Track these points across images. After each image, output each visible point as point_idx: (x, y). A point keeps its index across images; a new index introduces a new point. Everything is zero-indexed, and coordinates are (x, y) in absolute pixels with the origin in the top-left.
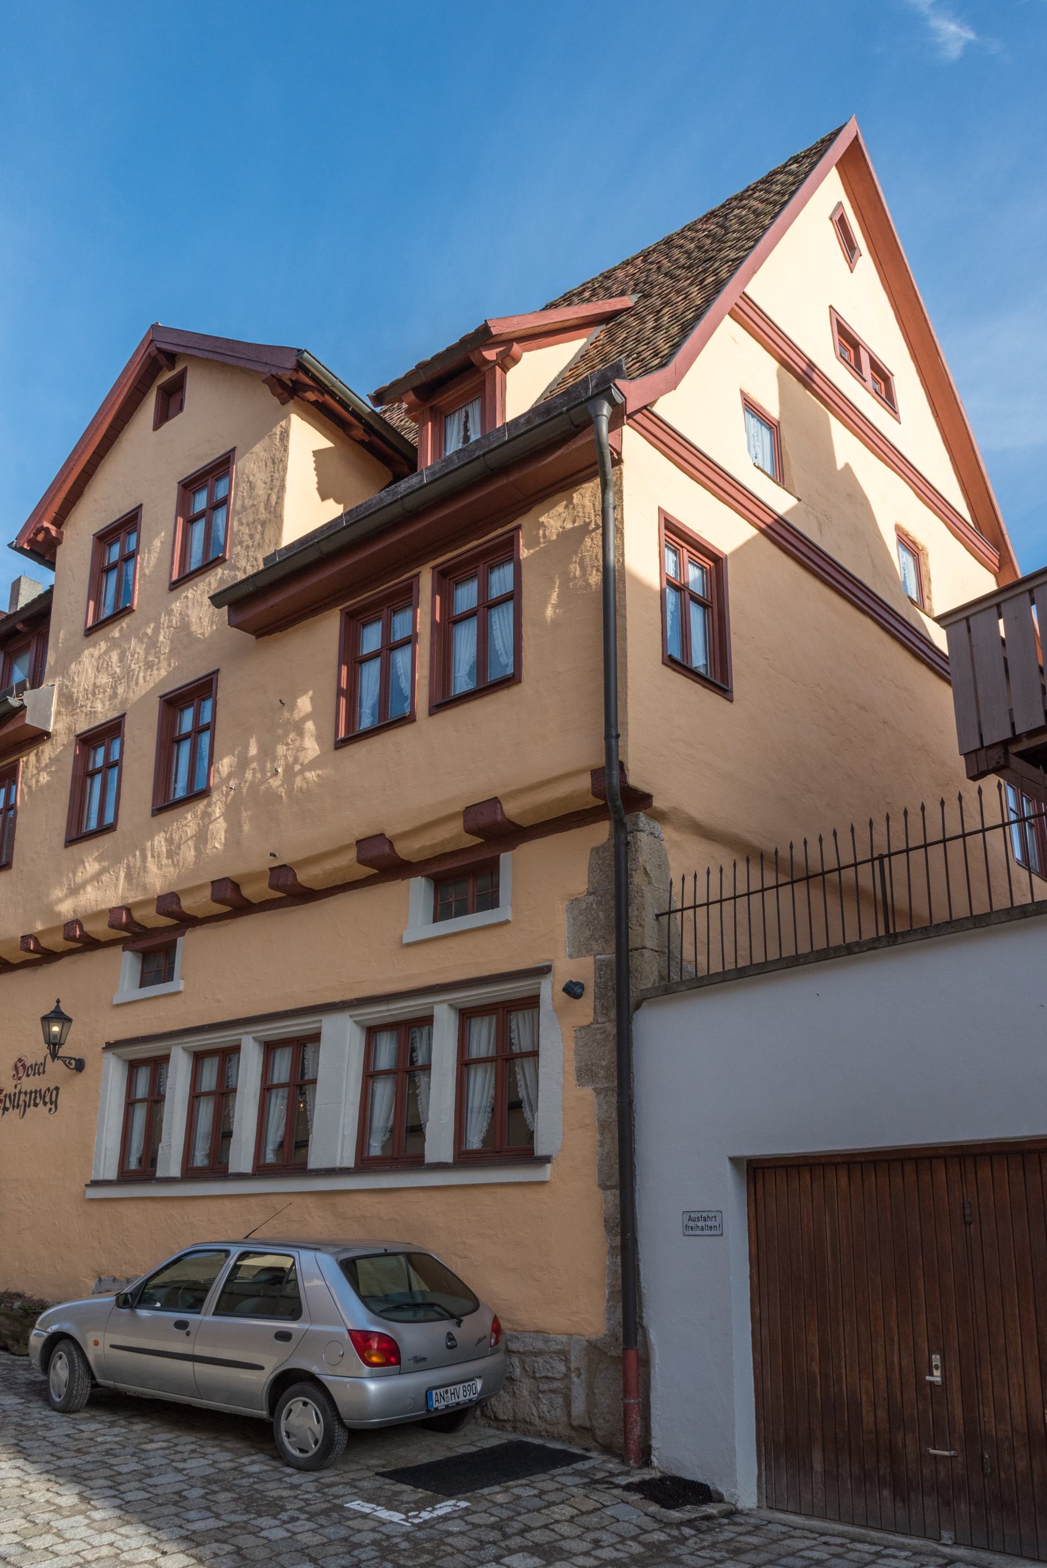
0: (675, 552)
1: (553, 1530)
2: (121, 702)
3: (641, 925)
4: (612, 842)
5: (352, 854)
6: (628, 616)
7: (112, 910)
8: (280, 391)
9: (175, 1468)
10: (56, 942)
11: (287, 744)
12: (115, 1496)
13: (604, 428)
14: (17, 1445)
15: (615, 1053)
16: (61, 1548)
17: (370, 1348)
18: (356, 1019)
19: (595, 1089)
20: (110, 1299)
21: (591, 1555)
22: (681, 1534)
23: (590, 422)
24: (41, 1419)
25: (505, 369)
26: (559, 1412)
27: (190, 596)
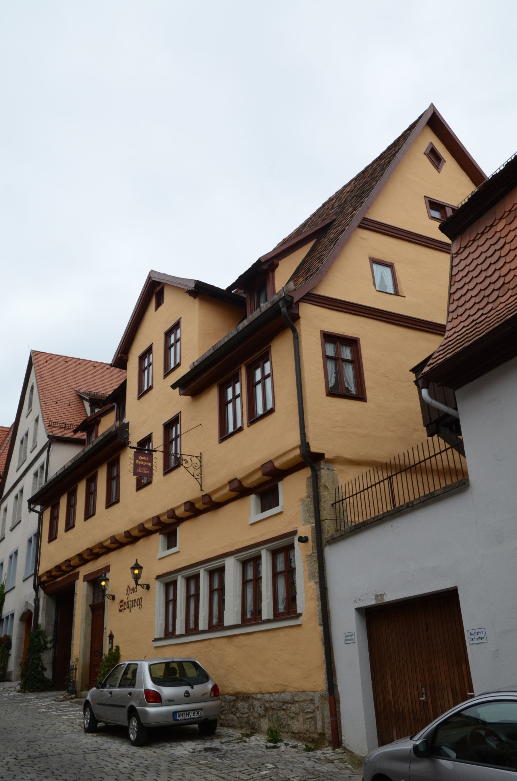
18: (237, 558)
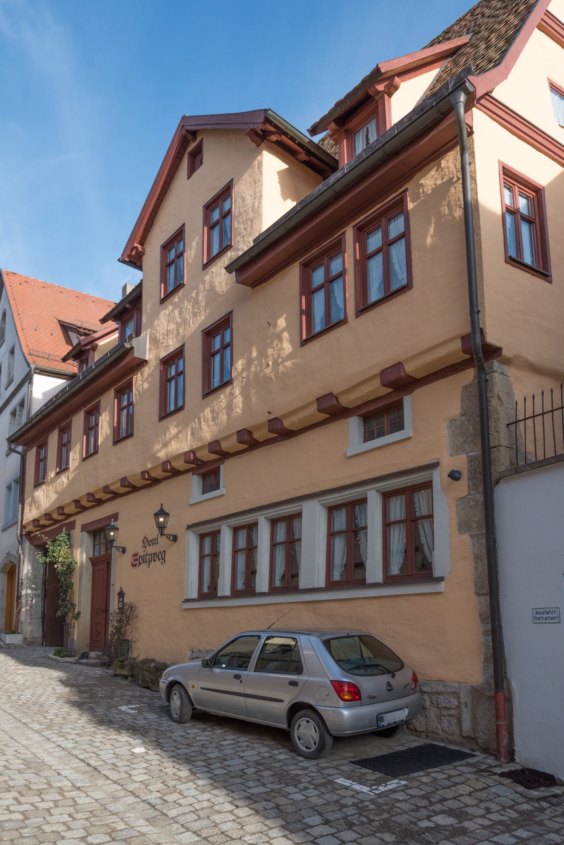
0: (510, 189)
1: (460, 801)
2: (182, 338)
3: (498, 432)
4: (477, 380)
5: (315, 407)
6: (482, 234)
7: (185, 453)
8: (256, 138)
9: (239, 755)
10: (158, 473)
11: (274, 348)
12: (208, 772)
13: (462, 110)
14: (156, 741)
15: (483, 513)
16: (182, 801)
17: (343, 691)
18: (322, 503)
19: (470, 536)
20: (198, 663)
21: (486, 818)
22: (540, 805)
23: (452, 109)
24: (168, 727)
25: (390, 95)
26: (454, 728)
27: (214, 271)
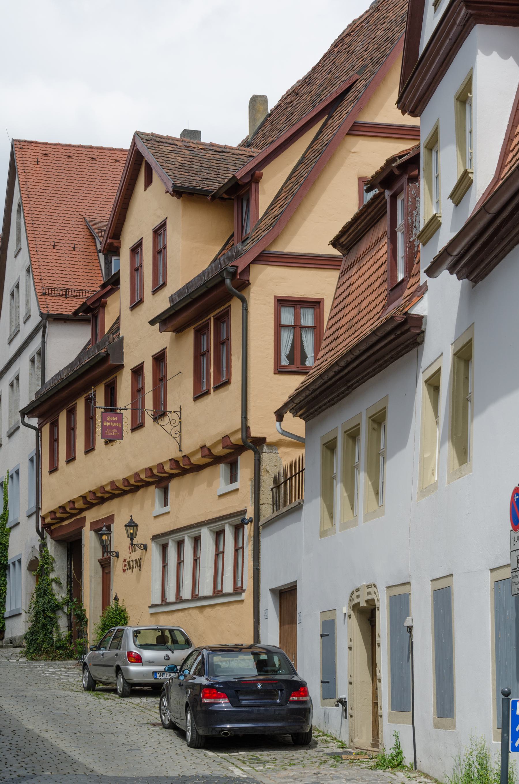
18: (210, 529)
